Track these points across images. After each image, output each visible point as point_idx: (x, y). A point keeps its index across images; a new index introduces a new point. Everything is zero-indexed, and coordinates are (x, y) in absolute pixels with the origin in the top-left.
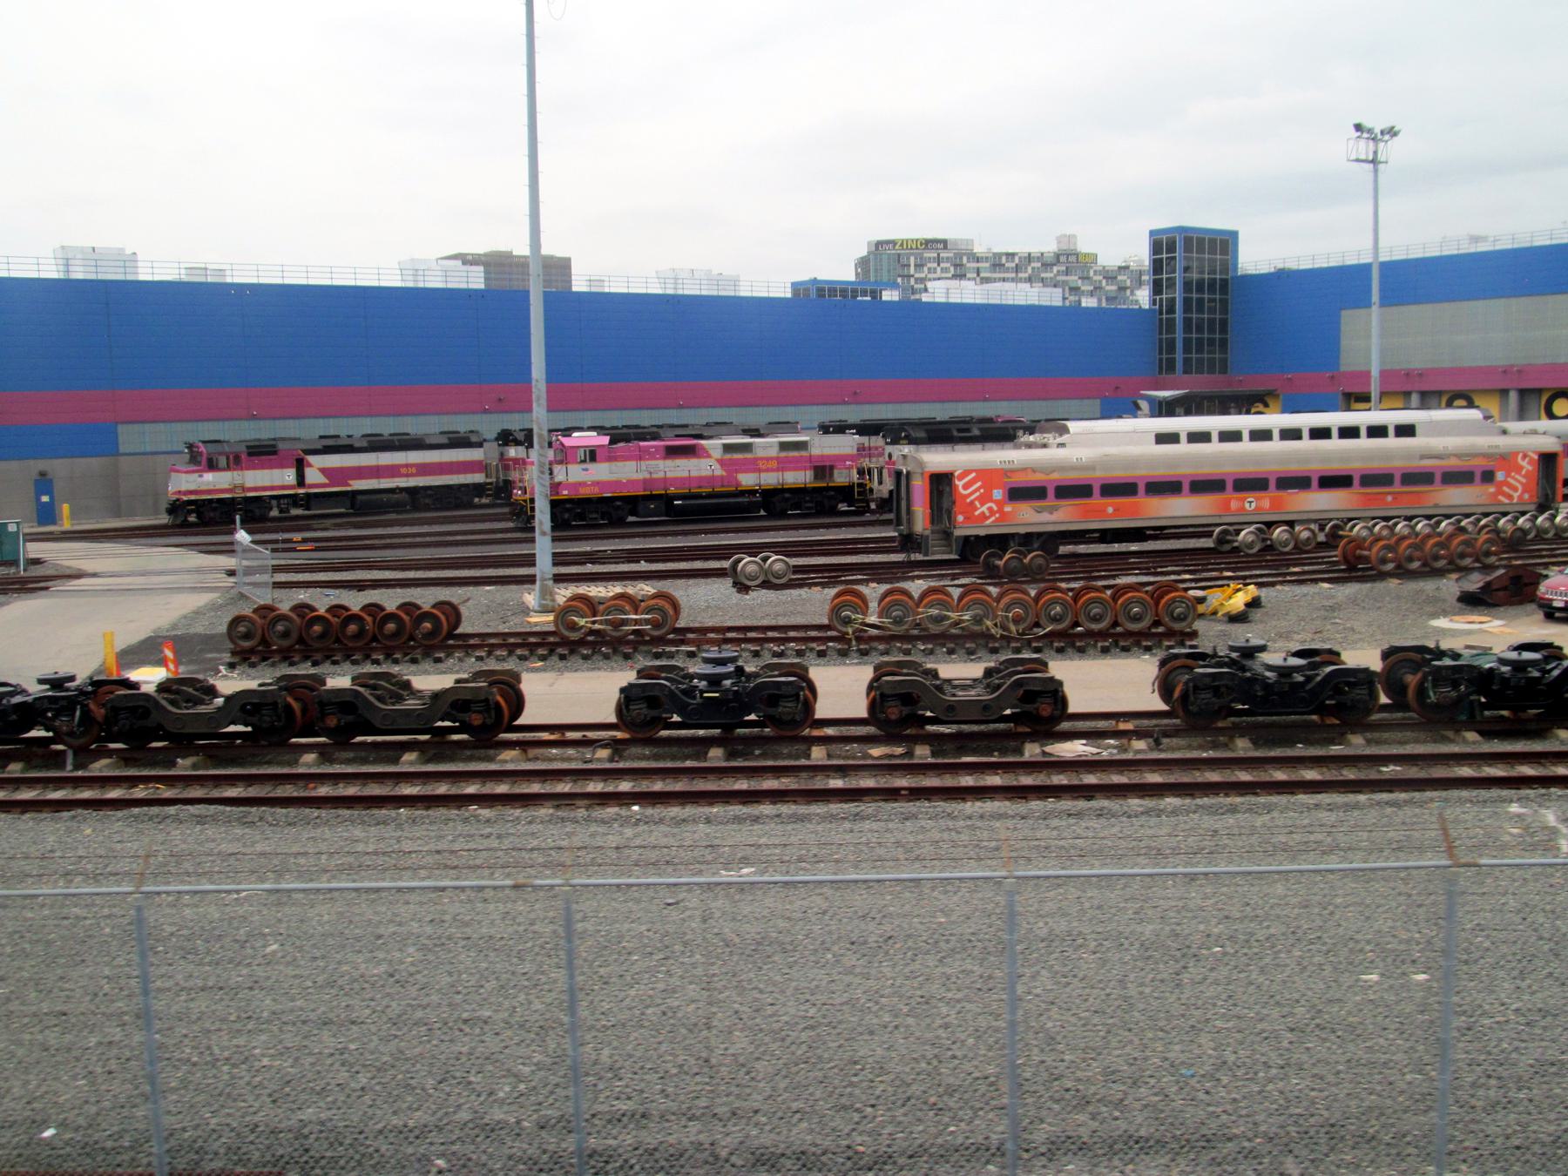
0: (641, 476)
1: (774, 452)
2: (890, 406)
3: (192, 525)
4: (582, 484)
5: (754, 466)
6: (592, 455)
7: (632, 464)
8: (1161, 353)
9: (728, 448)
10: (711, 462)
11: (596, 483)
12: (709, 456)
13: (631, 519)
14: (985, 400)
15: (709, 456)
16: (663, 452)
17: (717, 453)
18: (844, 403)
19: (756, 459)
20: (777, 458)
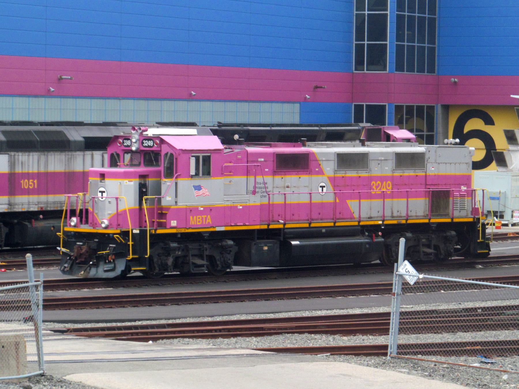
0: (256, 201)
1: (387, 169)
2: (276, 107)
3: (205, 274)
4: (193, 211)
5: (363, 189)
6: (206, 164)
7: (240, 180)
8: (360, 36)
9: (344, 160)
10: (325, 178)
11: (209, 210)
12: (321, 172)
13: (235, 268)
14: (190, 98)
15: (321, 172)
16: (271, 164)
17: (329, 168)
18: (48, 94)
19: (371, 179)
20: (392, 179)
